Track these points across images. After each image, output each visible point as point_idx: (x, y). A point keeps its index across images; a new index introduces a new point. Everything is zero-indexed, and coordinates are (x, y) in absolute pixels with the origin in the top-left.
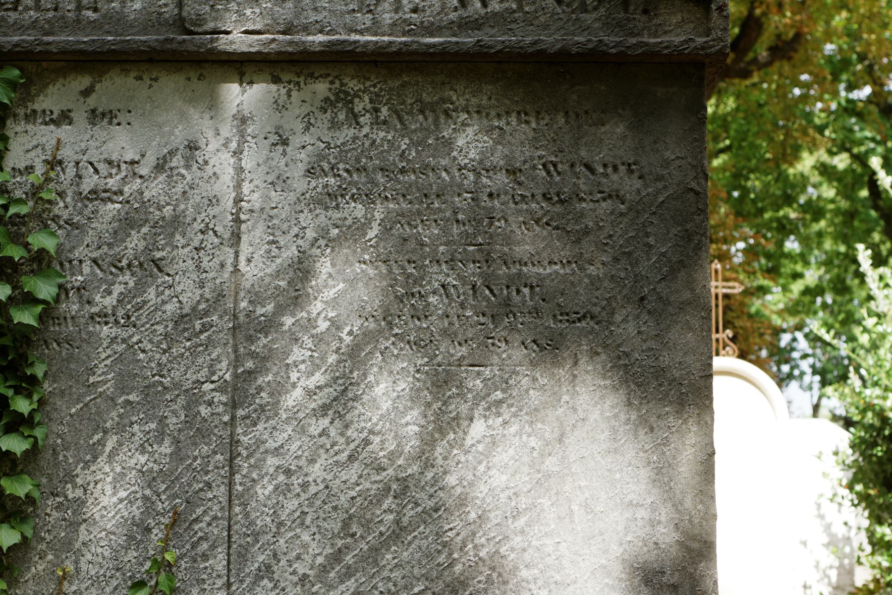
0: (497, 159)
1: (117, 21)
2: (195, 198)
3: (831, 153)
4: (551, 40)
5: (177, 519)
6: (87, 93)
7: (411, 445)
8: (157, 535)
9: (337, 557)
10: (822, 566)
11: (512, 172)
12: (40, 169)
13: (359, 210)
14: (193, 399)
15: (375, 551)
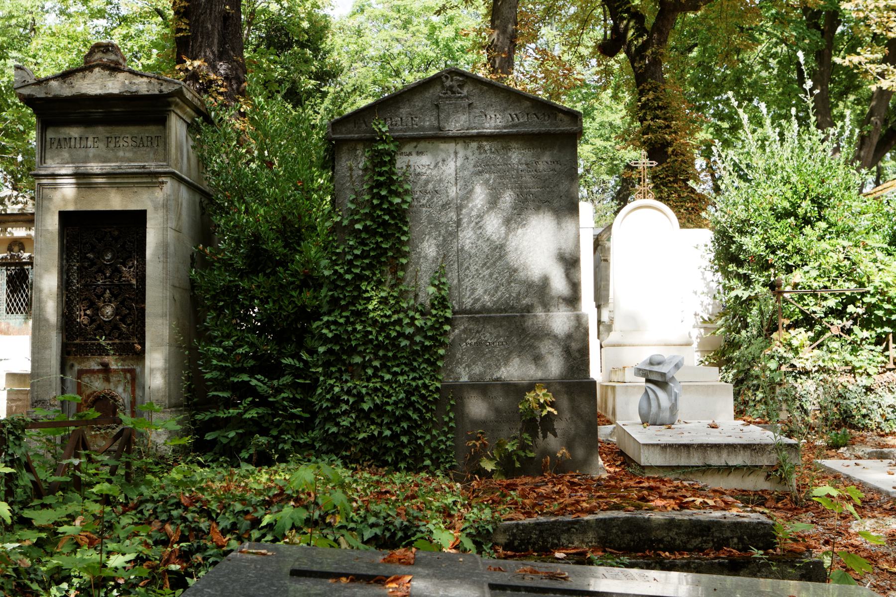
0: (523, 161)
1: (423, 128)
2: (445, 174)
3: (648, 100)
4: (536, 129)
5: (445, 256)
6: (415, 147)
7: (503, 235)
8: (440, 260)
9: (485, 264)
10: (705, 304)
11: (527, 164)
12: (405, 168)
13: (487, 176)
14: (447, 225)
15: (495, 262)
